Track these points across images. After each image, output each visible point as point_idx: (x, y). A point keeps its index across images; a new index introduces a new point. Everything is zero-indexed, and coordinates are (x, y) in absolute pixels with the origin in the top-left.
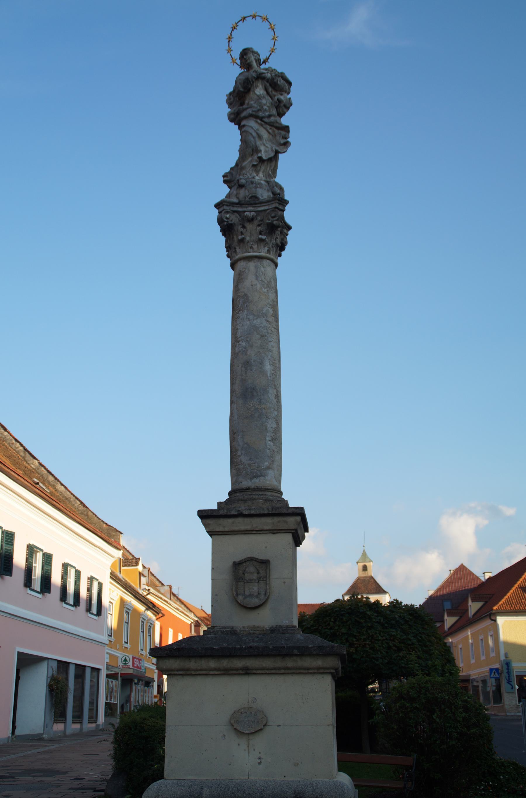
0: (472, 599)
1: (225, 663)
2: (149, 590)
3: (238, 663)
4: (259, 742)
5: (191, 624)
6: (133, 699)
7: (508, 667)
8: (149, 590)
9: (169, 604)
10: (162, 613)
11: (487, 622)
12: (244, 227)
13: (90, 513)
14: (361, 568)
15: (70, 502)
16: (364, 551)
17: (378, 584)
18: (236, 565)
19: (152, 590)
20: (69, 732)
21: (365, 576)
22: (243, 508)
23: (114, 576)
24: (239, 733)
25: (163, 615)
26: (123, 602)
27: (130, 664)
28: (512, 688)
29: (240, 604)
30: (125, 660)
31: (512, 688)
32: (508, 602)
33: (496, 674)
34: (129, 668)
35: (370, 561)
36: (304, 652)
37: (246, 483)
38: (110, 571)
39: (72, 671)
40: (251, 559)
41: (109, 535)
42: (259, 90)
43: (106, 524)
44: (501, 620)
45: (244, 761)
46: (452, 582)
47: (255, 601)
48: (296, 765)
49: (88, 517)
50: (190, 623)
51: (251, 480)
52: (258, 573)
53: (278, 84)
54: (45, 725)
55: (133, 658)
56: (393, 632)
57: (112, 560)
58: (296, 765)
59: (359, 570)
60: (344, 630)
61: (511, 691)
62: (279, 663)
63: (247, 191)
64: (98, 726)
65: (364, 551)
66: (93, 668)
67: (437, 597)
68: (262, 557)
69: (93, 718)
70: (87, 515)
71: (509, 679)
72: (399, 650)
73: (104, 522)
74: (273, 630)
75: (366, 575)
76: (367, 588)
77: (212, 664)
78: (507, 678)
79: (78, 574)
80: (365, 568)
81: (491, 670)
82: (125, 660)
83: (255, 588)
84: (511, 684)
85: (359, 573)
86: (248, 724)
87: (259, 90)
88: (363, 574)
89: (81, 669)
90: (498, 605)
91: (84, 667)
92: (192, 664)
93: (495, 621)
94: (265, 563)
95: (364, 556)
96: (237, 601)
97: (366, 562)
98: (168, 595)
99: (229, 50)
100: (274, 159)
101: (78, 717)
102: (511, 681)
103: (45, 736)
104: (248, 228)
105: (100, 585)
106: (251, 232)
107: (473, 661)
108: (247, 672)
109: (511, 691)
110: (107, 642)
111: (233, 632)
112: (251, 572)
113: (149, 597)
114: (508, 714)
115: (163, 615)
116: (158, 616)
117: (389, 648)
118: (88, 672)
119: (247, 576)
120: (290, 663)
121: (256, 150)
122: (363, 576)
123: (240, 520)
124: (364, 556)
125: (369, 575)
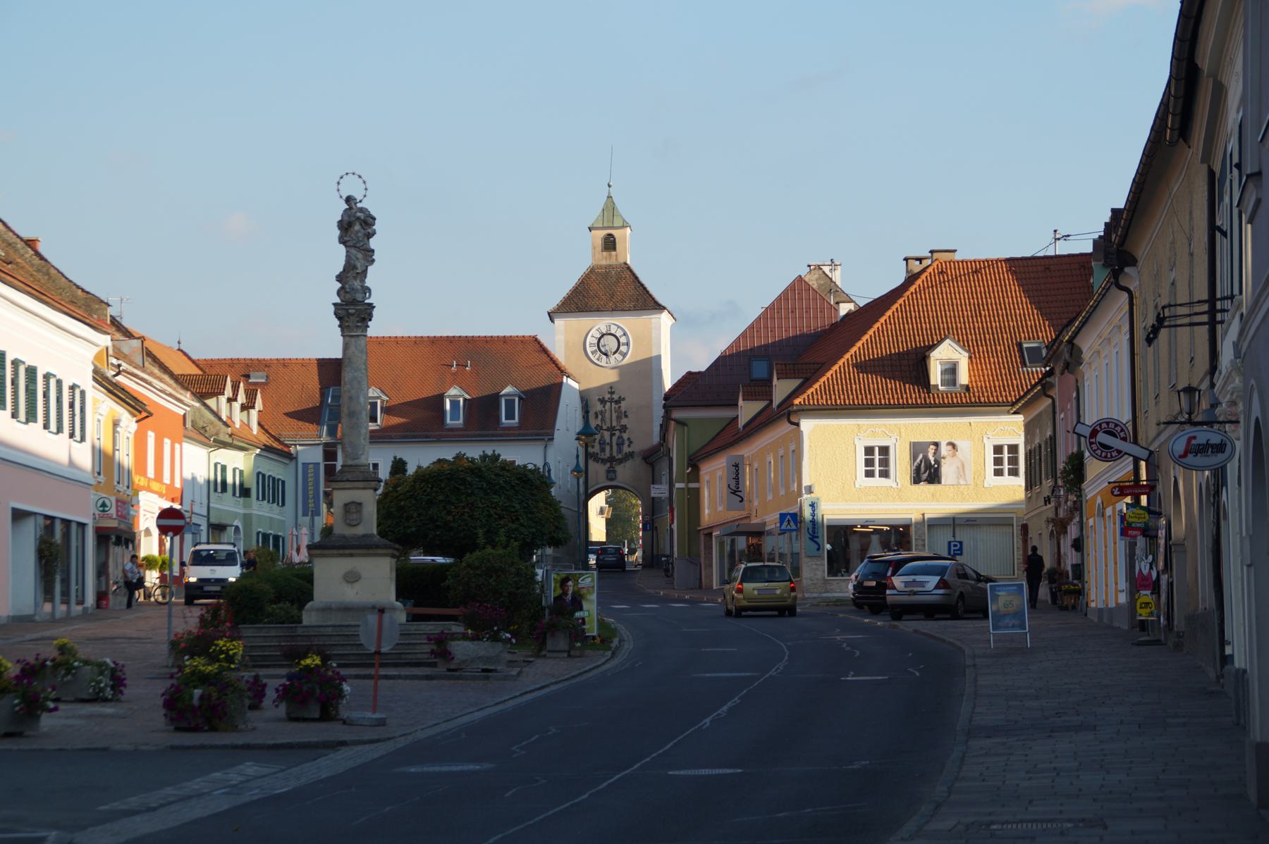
1: (341, 552)
2: (119, 366)
3: (347, 552)
4: (357, 585)
5: (184, 416)
6: (111, 569)
8: (119, 366)
9: (150, 384)
10: (146, 411)
11: (784, 428)
13: (53, 271)
14: (599, 243)
15: (16, 250)
16: (609, 197)
17: (642, 285)
18: (346, 505)
19: (125, 366)
20: (58, 615)
21: (608, 262)
22: (349, 476)
23: (100, 378)
24: (348, 582)
25: (150, 414)
27: (113, 511)
30: (104, 505)
32: (826, 390)
34: (111, 518)
35: (624, 226)
36: (377, 547)
37: (350, 462)
38: (92, 367)
39: (58, 527)
40: (353, 502)
41: (84, 307)
42: (357, 227)
43: (83, 290)
44: (808, 425)
45: (351, 594)
46: (773, 318)
49: (50, 278)
50: (182, 412)
53: (367, 221)
54: (36, 604)
55: (117, 501)
56: (496, 498)
57: (96, 350)
59: (594, 248)
60: (441, 498)
61: (816, 553)
62: (365, 551)
64: (85, 609)
65: (609, 197)
66: (63, 520)
67: (739, 354)
69: (81, 602)
70: (48, 274)
72: (501, 517)
73: (78, 287)
74: (364, 536)
75: (613, 262)
76: (612, 296)
77: (335, 552)
79: (59, 383)
80: (610, 244)
81: (783, 516)
82: (104, 505)
83: (355, 516)
85: (594, 255)
86: (352, 578)
87: (357, 227)
88: (604, 259)
89: (67, 523)
90: (805, 396)
91: (52, 518)
92: (326, 552)
93: (798, 425)
94: (360, 504)
95: (610, 208)
97: (613, 228)
98: (138, 360)
100: (365, 272)
101: (66, 601)
103: (37, 618)
105: (83, 393)
106: (352, 321)
107: (770, 497)
108: (351, 555)
109: (816, 553)
110: (93, 482)
111: (344, 537)
112: (353, 508)
113: (120, 379)
114: (807, 595)
115: (150, 414)
116: (140, 417)
117: (490, 516)
118: (74, 527)
120: (371, 551)
121: (355, 267)
122: (604, 263)
124: (610, 208)
125: (621, 261)
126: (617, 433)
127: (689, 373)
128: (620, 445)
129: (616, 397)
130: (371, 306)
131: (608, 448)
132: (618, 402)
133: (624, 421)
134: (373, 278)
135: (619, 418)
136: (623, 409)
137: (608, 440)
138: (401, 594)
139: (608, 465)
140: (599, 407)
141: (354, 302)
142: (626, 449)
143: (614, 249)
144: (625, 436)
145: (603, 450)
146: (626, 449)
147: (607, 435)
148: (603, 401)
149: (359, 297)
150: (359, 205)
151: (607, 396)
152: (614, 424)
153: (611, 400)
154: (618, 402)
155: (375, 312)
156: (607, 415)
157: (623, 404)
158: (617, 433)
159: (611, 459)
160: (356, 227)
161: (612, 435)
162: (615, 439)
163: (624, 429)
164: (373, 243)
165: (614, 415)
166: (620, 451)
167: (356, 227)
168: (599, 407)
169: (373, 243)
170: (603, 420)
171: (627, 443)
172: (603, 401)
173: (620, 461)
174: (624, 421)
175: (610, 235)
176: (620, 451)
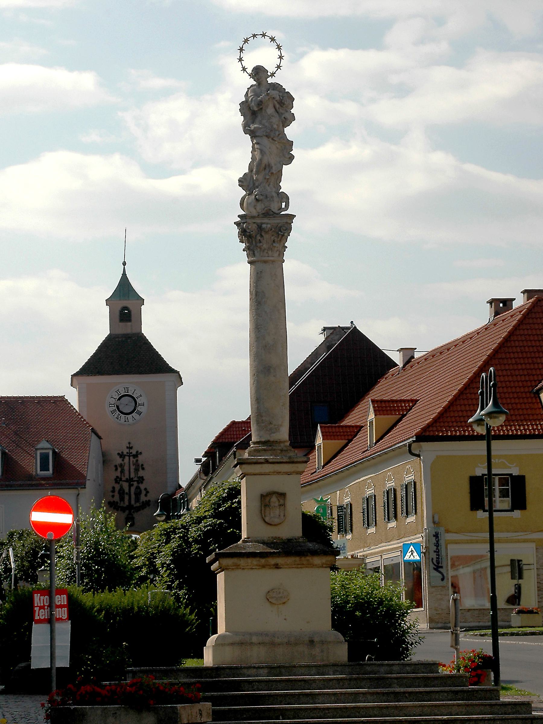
0: (375, 411)
7: (438, 542)
12: (261, 236)
18: (263, 497)
26: (486, 568)
28: (443, 579)
29: (265, 522)
31: (443, 579)
33: (415, 554)
40: (274, 493)
47: (277, 521)
48: (308, 622)
51: (270, 434)
52: (279, 502)
58: (308, 622)
63: (263, 205)
65: (124, 274)
68: (281, 491)
71: (438, 563)
78: (435, 561)
84: (440, 572)
96: (265, 522)
99: (244, 69)
102: (442, 567)
104: (265, 237)
119: (272, 504)
123: (266, 465)
126: (135, 484)
127: (234, 423)
128: (138, 494)
129: (134, 452)
130: (242, 241)
131: (127, 497)
132: (136, 456)
133: (141, 473)
134: (291, 180)
135: (137, 470)
136: (140, 462)
137: (127, 490)
138: (336, 625)
139: (127, 512)
140: (119, 461)
141: (268, 214)
142: (143, 498)
143: (130, 320)
144: (142, 487)
145: (122, 499)
146: (143, 498)
147: (126, 486)
148: (122, 455)
149: (274, 207)
150: (270, 80)
151: (126, 451)
152: (132, 475)
153: (129, 455)
154: (136, 456)
155: (295, 224)
156: (126, 468)
157: (140, 458)
158: (135, 484)
159: (130, 507)
160: (267, 110)
161: (130, 486)
162: (133, 489)
163: (141, 480)
164: (290, 132)
165: (133, 468)
166: (137, 499)
167: (267, 110)
168: (119, 461)
169: (290, 132)
170: (122, 472)
171: (144, 492)
172: (122, 455)
173: (138, 509)
174: (141, 473)
175: (126, 308)
176: (137, 499)
